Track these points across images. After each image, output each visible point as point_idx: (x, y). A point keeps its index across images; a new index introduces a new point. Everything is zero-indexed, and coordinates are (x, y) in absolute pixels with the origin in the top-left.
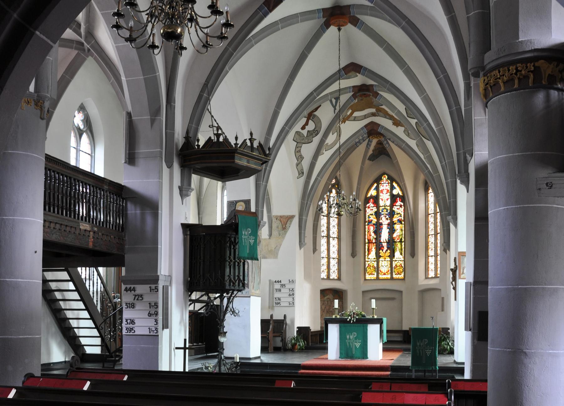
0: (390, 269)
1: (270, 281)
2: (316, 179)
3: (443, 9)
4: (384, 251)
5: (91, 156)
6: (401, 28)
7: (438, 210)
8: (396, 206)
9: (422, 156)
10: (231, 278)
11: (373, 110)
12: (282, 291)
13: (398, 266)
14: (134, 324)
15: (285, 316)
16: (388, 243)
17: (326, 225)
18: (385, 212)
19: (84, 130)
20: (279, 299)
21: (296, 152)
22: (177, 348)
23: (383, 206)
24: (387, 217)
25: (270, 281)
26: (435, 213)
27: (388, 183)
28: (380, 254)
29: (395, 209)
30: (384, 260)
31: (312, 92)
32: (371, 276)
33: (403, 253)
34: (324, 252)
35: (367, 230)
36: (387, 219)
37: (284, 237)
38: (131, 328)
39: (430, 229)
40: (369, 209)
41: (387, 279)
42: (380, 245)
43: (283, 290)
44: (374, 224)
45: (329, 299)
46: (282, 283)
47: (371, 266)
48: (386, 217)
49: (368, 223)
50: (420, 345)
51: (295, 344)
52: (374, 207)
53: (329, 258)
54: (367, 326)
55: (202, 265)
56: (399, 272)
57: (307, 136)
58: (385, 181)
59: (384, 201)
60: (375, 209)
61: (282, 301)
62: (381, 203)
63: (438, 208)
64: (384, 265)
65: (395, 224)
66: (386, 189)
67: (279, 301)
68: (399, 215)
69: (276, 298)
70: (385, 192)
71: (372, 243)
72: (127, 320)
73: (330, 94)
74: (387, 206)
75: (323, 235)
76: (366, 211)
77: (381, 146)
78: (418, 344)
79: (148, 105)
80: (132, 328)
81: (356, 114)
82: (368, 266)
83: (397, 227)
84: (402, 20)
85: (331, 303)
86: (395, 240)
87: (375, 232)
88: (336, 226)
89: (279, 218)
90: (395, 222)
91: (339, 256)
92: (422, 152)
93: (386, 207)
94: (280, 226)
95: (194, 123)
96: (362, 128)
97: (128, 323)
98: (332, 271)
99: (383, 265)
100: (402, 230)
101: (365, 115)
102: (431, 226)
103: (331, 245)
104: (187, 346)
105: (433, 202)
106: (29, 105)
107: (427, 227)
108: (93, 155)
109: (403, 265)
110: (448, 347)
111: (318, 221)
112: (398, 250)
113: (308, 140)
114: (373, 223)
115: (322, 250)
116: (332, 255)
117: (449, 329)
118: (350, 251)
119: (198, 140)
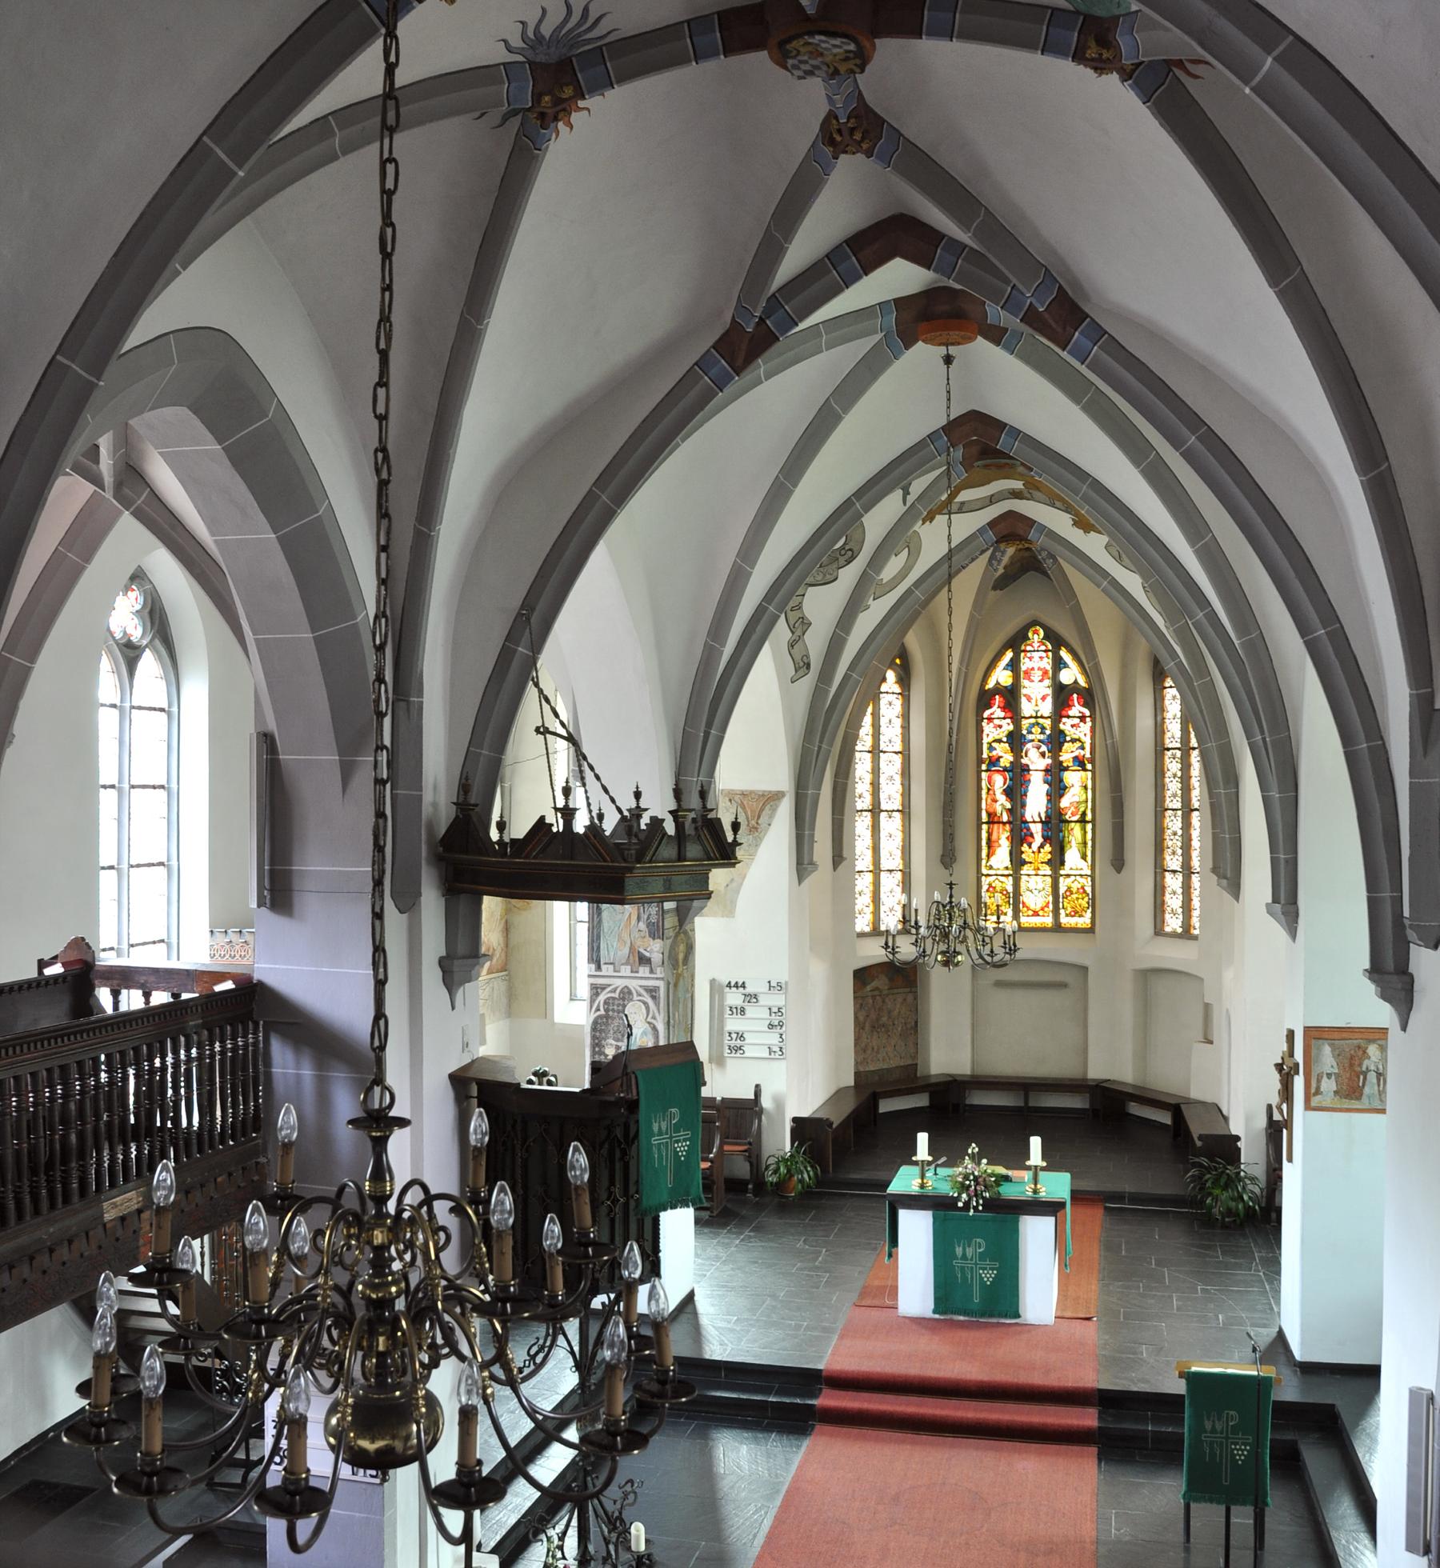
0: (1050, 899)
3: (1331, 406)
4: (1035, 846)
5: (169, 714)
6: (1180, 454)
7: (1194, 743)
8: (1068, 717)
9: (1160, 621)
10: (615, 1196)
11: (1018, 485)
12: (747, 1012)
13: (1074, 890)
15: (758, 1090)
16: (1046, 823)
17: (868, 778)
19: (145, 642)
20: (741, 1036)
23: (1031, 717)
24: (1041, 750)
26: (1186, 749)
27: (1046, 651)
28: (1023, 856)
29: (1066, 725)
30: (1034, 872)
31: (849, 498)
34: (862, 857)
35: (984, 784)
36: (1043, 755)
39: (1168, 793)
40: (991, 725)
41: (1043, 930)
42: (1022, 830)
43: (751, 1011)
44: (1005, 769)
45: (877, 989)
46: (750, 989)
47: (998, 889)
48: (1038, 748)
49: (988, 765)
50: (1214, 1430)
52: (1004, 718)
53: (876, 871)
54: (1018, 1221)
58: (1036, 645)
59: (1033, 701)
60: (1007, 726)
61: (746, 1042)
62: (1027, 708)
63: (1193, 735)
64: (1036, 889)
65: (1066, 769)
66: (1039, 669)
68: (1078, 744)
69: (730, 1033)
70: (1037, 675)
71: (999, 823)
73: (916, 589)
74: (1042, 717)
76: (982, 731)
77: (1027, 554)
78: (1208, 1425)
79: (330, 720)
81: (965, 495)
83: (1073, 778)
84: (1185, 431)
85: (884, 1002)
86: (1067, 817)
87: (1009, 792)
88: (898, 779)
89: (737, 798)
90: (1065, 765)
91: (904, 864)
92: (1160, 610)
93: (1040, 721)
96: (981, 531)
98: (887, 910)
100: (1086, 788)
101: (992, 495)
102: (1173, 786)
103: (883, 834)
105: (1179, 715)
108: (175, 709)
109: (1089, 890)
110: (1241, 1206)
112: (1074, 843)
113: (825, 575)
114: (1002, 764)
115: (858, 851)
116: (885, 864)
117: (1238, 1138)
118: (938, 851)
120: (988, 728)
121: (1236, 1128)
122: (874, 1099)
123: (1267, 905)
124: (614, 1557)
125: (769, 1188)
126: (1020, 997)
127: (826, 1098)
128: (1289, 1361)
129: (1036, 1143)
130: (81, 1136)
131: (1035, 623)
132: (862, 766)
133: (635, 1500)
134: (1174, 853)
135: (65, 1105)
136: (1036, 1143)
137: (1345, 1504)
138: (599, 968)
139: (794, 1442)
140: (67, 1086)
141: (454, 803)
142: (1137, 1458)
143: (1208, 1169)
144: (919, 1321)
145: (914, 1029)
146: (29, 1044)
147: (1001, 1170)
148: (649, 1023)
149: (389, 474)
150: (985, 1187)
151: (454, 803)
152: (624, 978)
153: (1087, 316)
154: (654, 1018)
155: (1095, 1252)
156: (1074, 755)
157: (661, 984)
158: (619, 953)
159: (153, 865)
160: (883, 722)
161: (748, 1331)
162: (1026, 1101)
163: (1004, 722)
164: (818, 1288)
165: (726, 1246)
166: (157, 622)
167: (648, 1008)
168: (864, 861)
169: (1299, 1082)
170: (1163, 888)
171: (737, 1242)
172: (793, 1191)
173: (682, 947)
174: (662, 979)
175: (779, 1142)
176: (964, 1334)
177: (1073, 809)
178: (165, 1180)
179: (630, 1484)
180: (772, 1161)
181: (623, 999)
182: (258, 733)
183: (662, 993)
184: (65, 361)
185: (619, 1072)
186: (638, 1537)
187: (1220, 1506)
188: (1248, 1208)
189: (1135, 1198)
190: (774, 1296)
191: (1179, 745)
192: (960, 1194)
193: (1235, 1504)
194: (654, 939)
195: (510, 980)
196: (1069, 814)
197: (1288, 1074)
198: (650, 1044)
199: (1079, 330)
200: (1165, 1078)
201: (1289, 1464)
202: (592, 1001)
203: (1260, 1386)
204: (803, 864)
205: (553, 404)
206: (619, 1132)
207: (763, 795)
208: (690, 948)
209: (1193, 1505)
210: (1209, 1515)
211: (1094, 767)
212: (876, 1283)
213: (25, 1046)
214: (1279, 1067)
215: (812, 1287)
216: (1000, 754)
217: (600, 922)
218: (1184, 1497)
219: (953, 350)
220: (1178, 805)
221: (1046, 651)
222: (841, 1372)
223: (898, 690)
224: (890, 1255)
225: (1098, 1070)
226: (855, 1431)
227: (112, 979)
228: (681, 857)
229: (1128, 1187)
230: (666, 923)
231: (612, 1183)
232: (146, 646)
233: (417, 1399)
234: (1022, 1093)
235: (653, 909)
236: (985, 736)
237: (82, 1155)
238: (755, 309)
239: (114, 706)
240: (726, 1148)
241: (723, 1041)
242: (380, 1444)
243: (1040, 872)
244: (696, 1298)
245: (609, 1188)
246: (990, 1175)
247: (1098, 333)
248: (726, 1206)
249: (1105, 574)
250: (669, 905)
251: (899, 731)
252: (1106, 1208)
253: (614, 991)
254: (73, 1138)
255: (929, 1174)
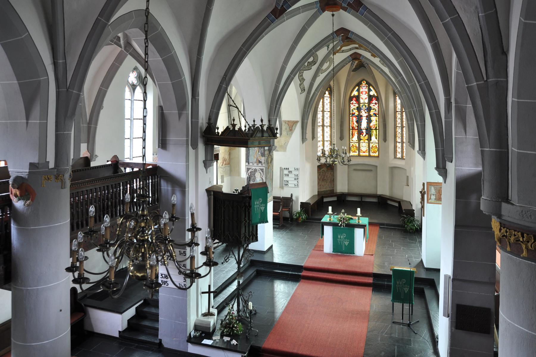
0: (368, 149)
1: (281, 168)
2: (314, 93)
4: (364, 135)
7: (404, 110)
8: (372, 103)
9: (393, 80)
11: (357, 46)
13: (374, 146)
14: (167, 279)
16: (367, 130)
17: (321, 118)
18: (364, 108)
19: (137, 84)
20: (288, 182)
21: (299, 76)
22: (203, 293)
23: (363, 103)
25: (281, 168)
26: (402, 112)
28: (361, 138)
29: (372, 105)
32: (354, 153)
33: (378, 137)
35: (351, 120)
36: (366, 113)
37: (290, 137)
38: (165, 281)
39: (398, 123)
40: (353, 105)
43: (290, 175)
44: (356, 116)
46: (289, 170)
47: (354, 146)
48: (365, 111)
50: (399, 284)
51: (299, 216)
52: (356, 103)
55: (223, 222)
56: (375, 151)
57: (307, 66)
58: (364, 85)
59: (363, 99)
60: (357, 105)
61: (289, 183)
62: (362, 101)
64: (364, 146)
65: (372, 116)
66: (365, 91)
67: (287, 183)
69: (285, 181)
70: (364, 93)
71: (355, 129)
72: (162, 275)
74: (365, 103)
75: (319, 125)
76: (350, 107)
77: (361, 63)
78: (398, 283)
80: (166, 281)
81: (344, 48)
82: (352, 146)
83: (373, 119)
87: (357, 122)
88: (329, 118)
89: (287, 122)
90: (371, 115)
91: (331, 139)
93: (365, 104)
94: (288, 128)
95: (215, 109)
97: (162, 276)
99: (363, 145)
100: (377, 121)
101: (350, 48)
102: (399, 121)
103: (325, 132)
104: (212, 290)
105: (400, 103)
106: (50, 181)
107: (395, 121)
109: (378, 146)
110: (414, 228)
111: (315, 117)
112: (374, 135)
113: (308, 68)
114: (355, 115)
115: (318, 136)
116: (326, 139)
117: (414, 210)
118: (339, 136)
119: (218, 128)
120: (352, 106)
121: (414, 208)
122: (322, 198)
123: (417, 151)
124: (246, 310)
125: (294, 220)
126: (360, 173)
127: (311, 197)
128: (423, 267)
129: (359, 210)
130: (112, 203)
131: (364, 80)
132: (320, 115)
133: (252, 297)
134: (399, 138)
135: (108, 195)
136: (359, 210)
137: (435, 304)
138: (249, 164)
139: (295, 284)
140: (108, 191)
141: (207, 123)
142: (382, 291)
143: (406, 218)
144: (329, 254)
145: (333, 181)
146: (98, 180)
147: (350, 216)
148: (261, 178)
149: (148, 44)
150: (346, 220)
151: (207, 123)
152: (254, 166)
153: (363, 4)
154: (262, 176)
155: (376, 238)
156: (374, 113)
157: (264, 168)
158: (254, 160)
159: (139, 138)
160: (325, 104)
161: (285, 256)
162: (361, 199)
163: (356, 104)
164: (304, 245)
165: (282, 234)
166: (140, 80)
167: (261, 174)
168: (320, 138)
169: (426, 196)
170: (396, 146)
171: (285, 233)
172: (301, 220)
173: (270, 159)
174: (264, 167)
175: (297, 208)
176: (340, 258)
177: (373, 126)
178: (92, 210)
179: (250, 293)
180: (295, 213)
181: (255, 172)
182: (159, 106)
183: (264, 170)
184: (100, 18)
185: (247, 189)
186: (250, 306)
187: (401, 304)
188: (416, 228)
189: (387, 225)
190: (293, 247)
191: (400, 111)
192: (339, 222)
193: (404, 303)
194: (262, 157)
195: (230, 167)
196: (372, 127)
197: (423, 194)
198: (262, 182)
199: (361, 7)
200: (397, 194)
201: (421, 294)
202: (247, 172)
203: (411, 273)
204: (304, 139)
205: (231, 27)
206: (247, 204)
207: (293, 122)
208: (272, 159)
209: (394, 303)
210: (398, 306)
211: (379, 116)
212: (319, 244)
213: (98, 181)
214: (421, 192)
215: (303, 245)
216: (355, 112)
217: (249, 153)
218: (392, 301)
219: (334, 13)
220: (400, 126)
221: (366, 87)
222: (308, 266)
223: (329, 96)
224: (322, 237)
225: (380, 192)
226: (311, 281)
227: (124, 165)
228: (262, 136)
229: (386, 222)
230: (265, 153)
231: (245, 217)
232: (138, 85)
233: (147, 263)
234: (360, 197)
235: (262, 150)
236: (351, 108)
237: (116, 207)
238: (280, 3)
239: (130, 100)
240: (283, 209)
241: (283, 183)
242: (142, 274)
243: (365, 142)
244: (273, 247)
245: (244, 218)
246: (347, 218)
247: (366, 8)
248: (283, 224)
249: (379, 68)
250: (266, 148)
251: (329, 106)
252: (380, 227)
253: (252, 170)
254: (110, 203)
255: (332, 217)
